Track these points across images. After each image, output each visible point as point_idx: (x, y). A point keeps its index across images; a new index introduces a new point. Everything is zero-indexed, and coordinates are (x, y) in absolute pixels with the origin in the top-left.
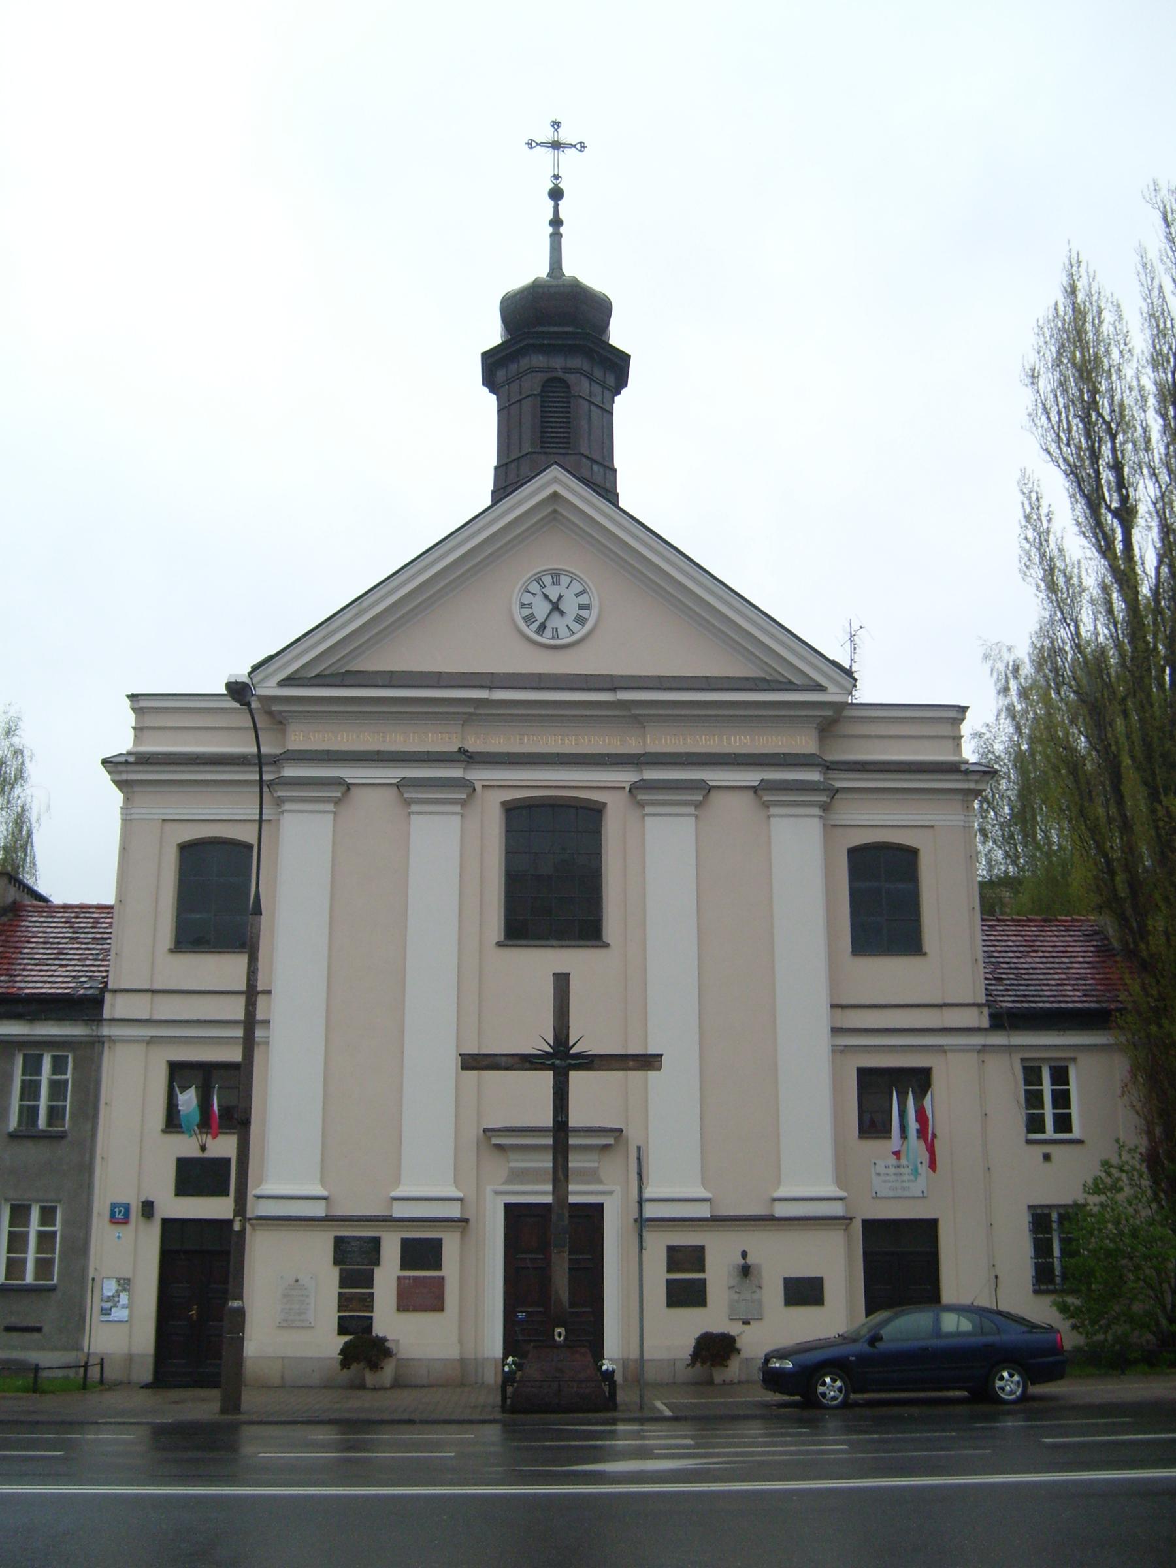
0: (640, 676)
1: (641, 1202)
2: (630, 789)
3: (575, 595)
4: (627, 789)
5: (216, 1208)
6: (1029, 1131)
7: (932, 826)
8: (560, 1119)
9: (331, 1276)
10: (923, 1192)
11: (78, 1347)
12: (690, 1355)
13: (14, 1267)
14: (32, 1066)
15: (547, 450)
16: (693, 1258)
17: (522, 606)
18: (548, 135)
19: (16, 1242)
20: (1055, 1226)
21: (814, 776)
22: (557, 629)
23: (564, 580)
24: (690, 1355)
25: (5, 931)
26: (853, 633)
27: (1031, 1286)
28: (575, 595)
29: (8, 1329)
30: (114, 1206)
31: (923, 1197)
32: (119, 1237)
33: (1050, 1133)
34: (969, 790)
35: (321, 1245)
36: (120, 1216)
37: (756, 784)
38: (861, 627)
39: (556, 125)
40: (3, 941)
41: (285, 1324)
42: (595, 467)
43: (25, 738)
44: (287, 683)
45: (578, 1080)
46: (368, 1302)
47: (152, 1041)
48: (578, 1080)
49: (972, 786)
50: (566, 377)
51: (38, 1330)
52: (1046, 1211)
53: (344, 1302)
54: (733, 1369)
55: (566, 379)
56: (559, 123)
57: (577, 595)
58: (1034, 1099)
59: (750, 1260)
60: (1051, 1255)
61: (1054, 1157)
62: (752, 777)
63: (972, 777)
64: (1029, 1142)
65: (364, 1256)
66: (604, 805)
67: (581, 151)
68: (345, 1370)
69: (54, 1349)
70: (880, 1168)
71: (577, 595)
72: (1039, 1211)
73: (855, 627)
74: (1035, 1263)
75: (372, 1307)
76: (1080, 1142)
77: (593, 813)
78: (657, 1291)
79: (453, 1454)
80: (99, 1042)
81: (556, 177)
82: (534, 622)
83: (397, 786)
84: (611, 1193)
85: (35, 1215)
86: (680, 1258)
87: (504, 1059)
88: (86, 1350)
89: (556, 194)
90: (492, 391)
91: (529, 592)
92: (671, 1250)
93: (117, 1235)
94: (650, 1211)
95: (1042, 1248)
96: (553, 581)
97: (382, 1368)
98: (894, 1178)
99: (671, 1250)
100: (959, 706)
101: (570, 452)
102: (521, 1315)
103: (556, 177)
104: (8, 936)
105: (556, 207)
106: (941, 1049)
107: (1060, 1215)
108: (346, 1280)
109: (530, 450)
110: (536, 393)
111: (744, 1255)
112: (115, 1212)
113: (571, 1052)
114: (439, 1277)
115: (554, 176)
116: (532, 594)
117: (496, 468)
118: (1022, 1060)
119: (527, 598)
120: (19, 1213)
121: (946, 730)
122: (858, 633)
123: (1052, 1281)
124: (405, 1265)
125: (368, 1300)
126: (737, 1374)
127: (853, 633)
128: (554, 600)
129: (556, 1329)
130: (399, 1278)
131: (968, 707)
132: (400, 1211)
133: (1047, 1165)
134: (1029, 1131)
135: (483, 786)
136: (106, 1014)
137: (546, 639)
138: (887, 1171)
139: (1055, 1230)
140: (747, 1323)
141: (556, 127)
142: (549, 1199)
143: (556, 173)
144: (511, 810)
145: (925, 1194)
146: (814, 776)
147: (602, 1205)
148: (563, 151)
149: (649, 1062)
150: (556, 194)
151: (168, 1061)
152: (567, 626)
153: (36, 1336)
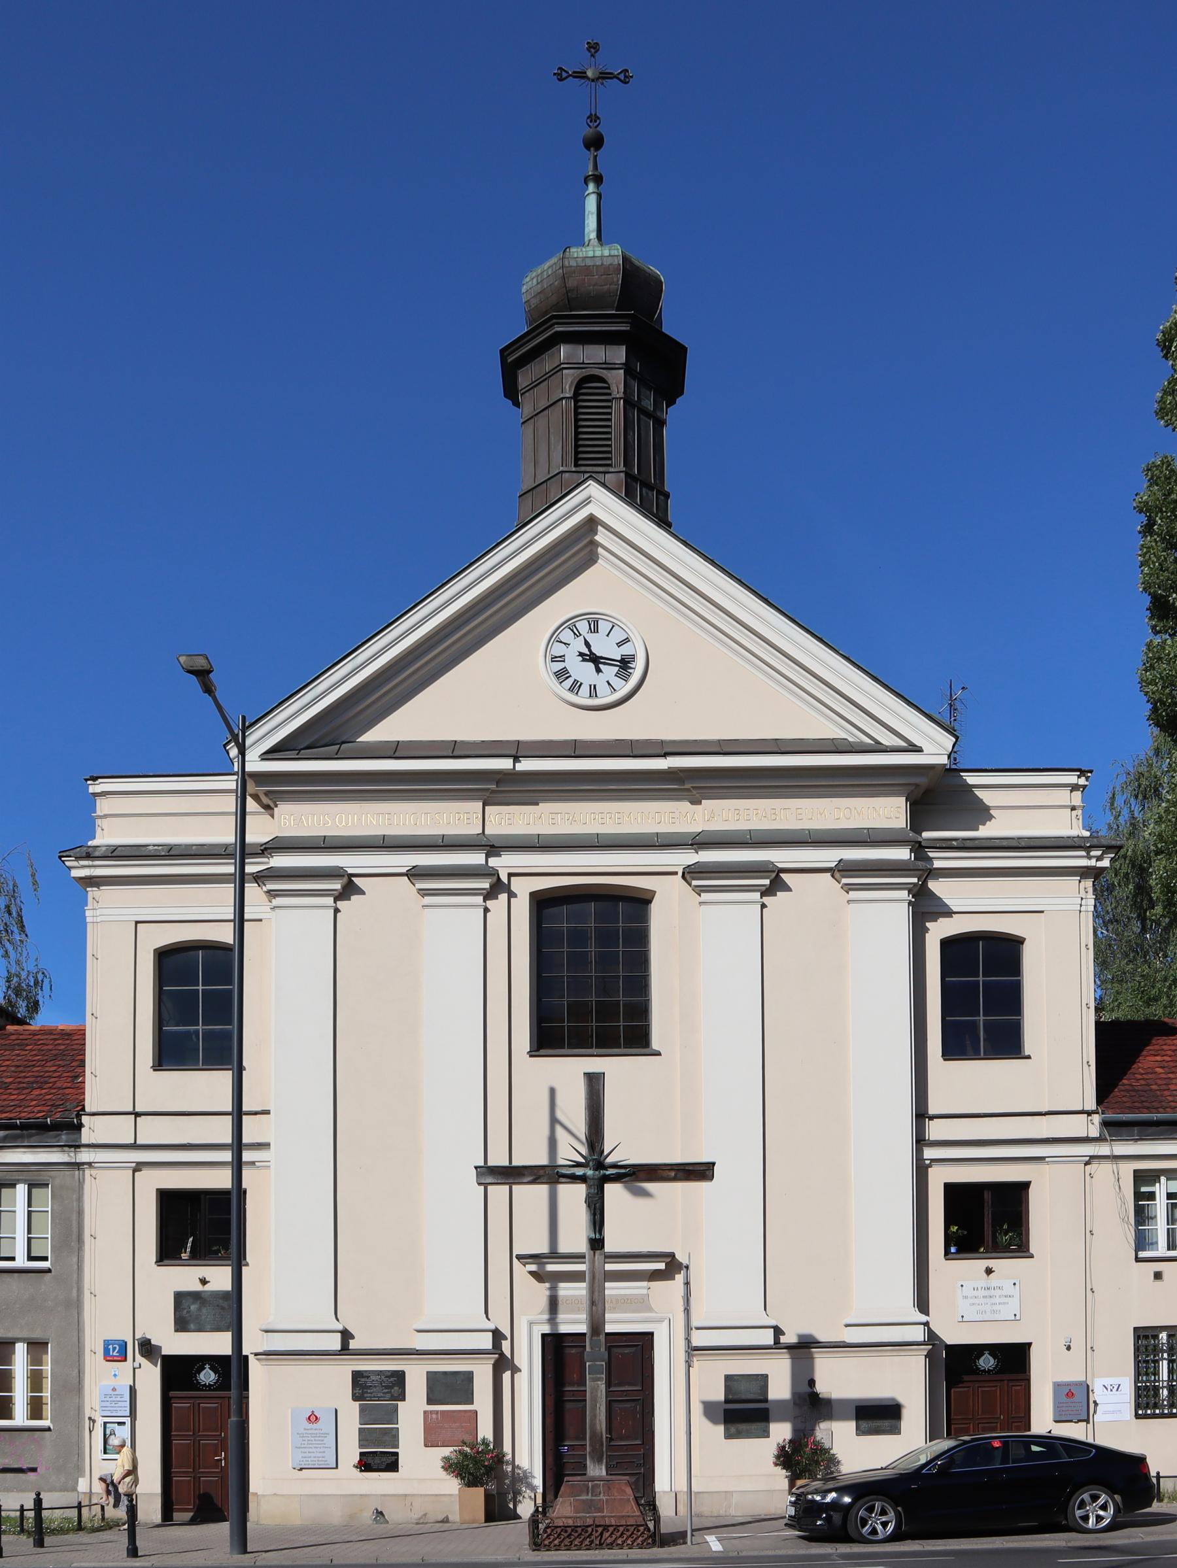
2: (683, 873)
3: (617, 644)
4: (680, 874)
5: (218, 1344)
9: (351, 1413)
10: (1015, 1315)
21: (476, 858)
22: (581, 684)
28: (617, 644)
32: (115, 1375)
35: (341, 1374)
36: (116, 1352)
44: (270, 756)
57: (619, 644)
62: (830, 856)
66: (653, 893)
71: (619, 644)
77: (640, 902)
81: (594, 118)
82: (567, 678)
91: (561, 642)
93: (113, 1373)
94: (699, 1339)
96: (590, 628)
98: (982, 1301)
109: (561, 469)
110: (568, 395)
114: (470, 1411)
115: (590, 117)
116: (565, 644)
119: (558, 650)
130: (425, 1412)
133: (1158, 1283)
137: (583, 699)
138: (975, 1293)
144: (542, 903)
145: (1018, 1318)
146: (476, 858)
147: (652, 1334)
148: (602, 84)
151: (157, 1189)
152: (608, 682)
153: (31, 1475)
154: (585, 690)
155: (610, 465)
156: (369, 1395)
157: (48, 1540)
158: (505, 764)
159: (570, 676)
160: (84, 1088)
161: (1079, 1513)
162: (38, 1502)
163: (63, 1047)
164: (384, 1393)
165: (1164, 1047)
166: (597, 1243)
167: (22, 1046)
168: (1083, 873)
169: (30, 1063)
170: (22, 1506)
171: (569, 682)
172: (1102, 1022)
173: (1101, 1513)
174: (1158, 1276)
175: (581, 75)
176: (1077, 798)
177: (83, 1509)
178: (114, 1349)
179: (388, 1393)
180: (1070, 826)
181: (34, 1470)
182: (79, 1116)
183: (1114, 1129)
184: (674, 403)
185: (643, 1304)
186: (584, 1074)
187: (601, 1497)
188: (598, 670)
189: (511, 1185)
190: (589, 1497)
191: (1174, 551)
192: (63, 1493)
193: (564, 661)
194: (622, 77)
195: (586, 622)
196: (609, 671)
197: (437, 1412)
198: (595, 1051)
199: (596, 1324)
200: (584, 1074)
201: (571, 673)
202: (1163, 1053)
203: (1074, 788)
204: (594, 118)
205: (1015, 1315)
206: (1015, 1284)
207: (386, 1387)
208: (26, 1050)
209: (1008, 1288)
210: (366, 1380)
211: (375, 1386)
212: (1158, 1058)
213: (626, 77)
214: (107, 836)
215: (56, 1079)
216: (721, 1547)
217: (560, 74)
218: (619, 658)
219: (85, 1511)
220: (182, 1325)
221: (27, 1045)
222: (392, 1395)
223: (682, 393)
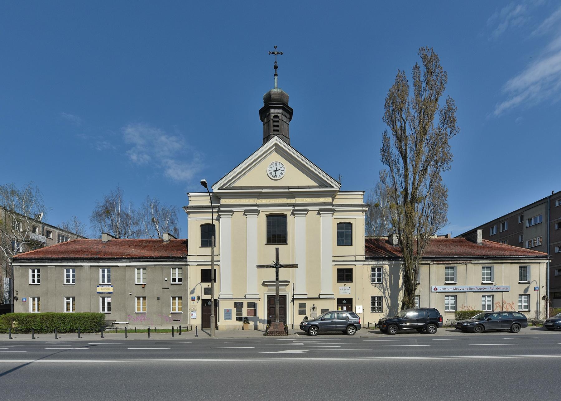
1: (293, 295)
11: (187, 324)
16: (302, 306)
17: (269, 171)
21: (331, 207)
23: (278, 164)
33: (376, 282)
35: (232, 303)
39: (275, 47)
47: (198, 265)
60: (375, 305)
67: (281, 55)
70: (341, 288)
77: (285, 216)
78: (296, 312)
81: (276, 62)
84: (288, 293)
86: (302, 306)
89: (276, 67)
106: (355, 265)
111: (314, 305)
126: (49, 272)
128: (275, 172)
132: (247, 297)
135: (262, 211)
142: (275, 295)
146: (331, 207)
149: (295, 266)
150: (276, 67)
155: (279, 133)
157: (182, 333)
158: (287, 190)
161: (349, 329)
162: (180, 327)
166: (277, 279)
167: (177, 243)
168: (363, 211)
173: (314, 333)
175: (273, 53)
176: (362, 197)
180: (361, 202)
181: (179, 320)
183: (367, 259)
185: (284, 290)
188: (274, 171)
189: (295, 268)
194: (281, 53)
196: (274, 173)
198: (277, 244)
199: (277, 293)
203: (362, 195)
204: (276, 62)
209: (348, 287)
214: (191, 204)
219: (188, 328)
220: (205, 294)
223: (292, 119)
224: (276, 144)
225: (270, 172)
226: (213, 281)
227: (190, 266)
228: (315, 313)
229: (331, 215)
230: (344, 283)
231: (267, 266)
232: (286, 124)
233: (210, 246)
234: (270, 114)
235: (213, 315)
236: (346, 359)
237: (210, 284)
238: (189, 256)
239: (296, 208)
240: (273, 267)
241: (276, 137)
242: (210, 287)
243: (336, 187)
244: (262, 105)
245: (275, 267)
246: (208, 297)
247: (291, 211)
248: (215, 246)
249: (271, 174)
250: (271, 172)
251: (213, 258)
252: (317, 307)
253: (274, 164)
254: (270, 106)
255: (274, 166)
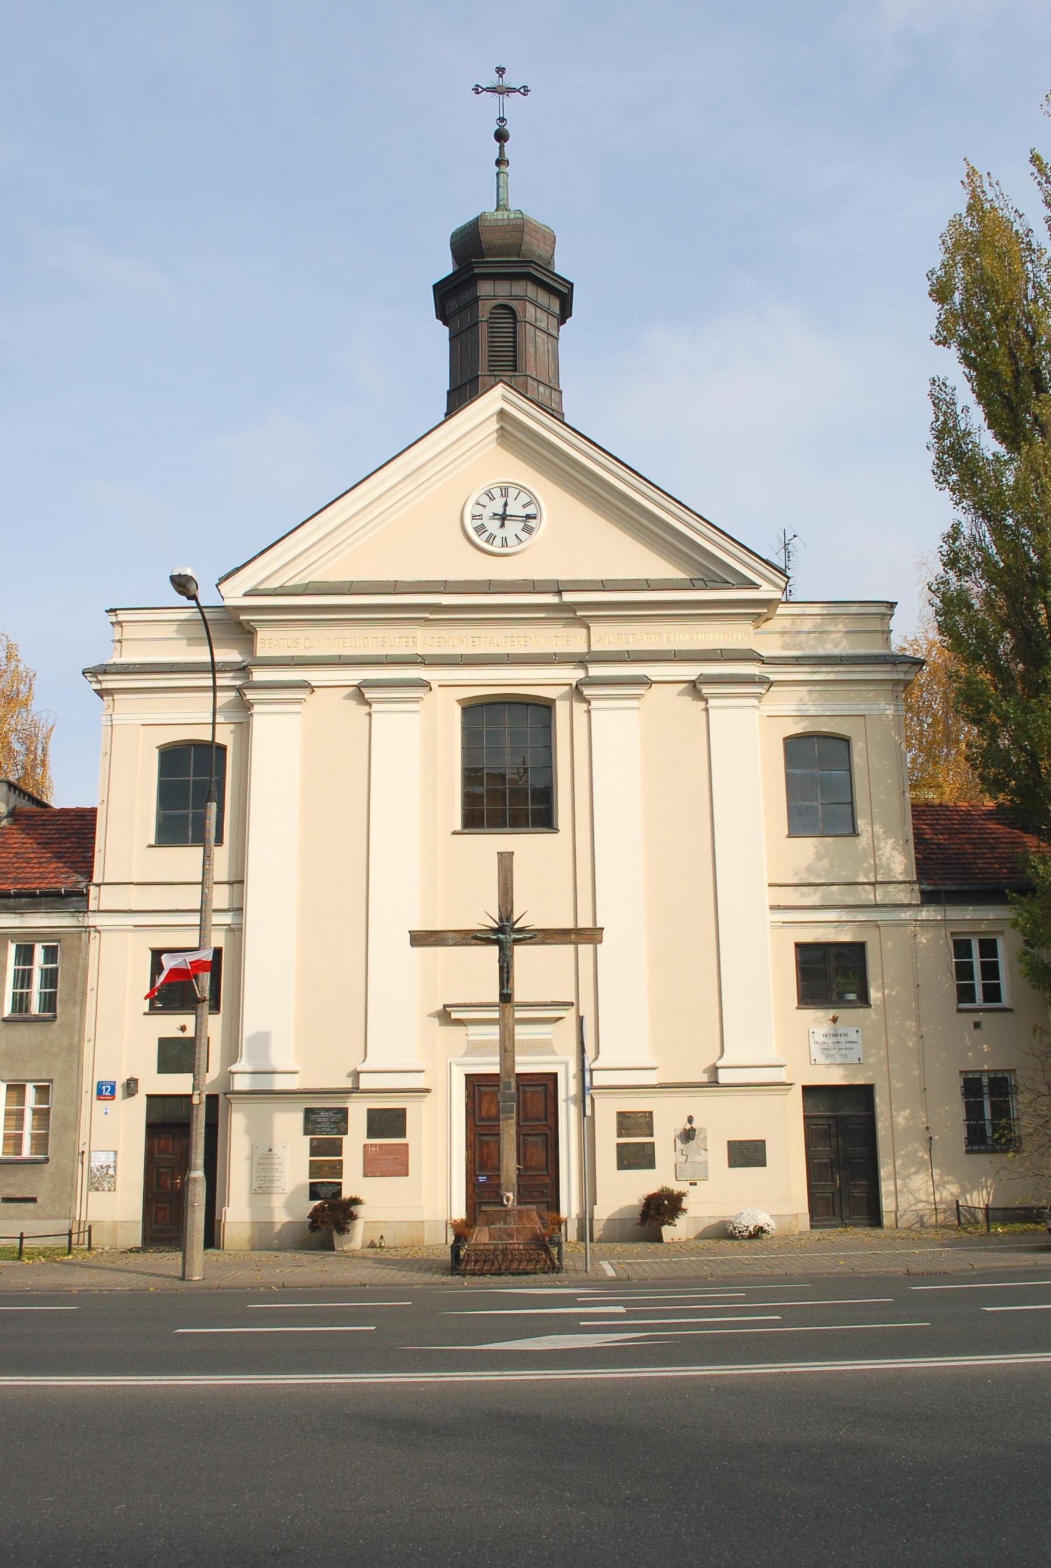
0: (584, 581)
6: (960, 1001)
7: (864, 715)
8: (503, 992)
10: (859, 1059)
11: (70, 1216)
12: (640, 1215)
13: (14, 1141)
14: (25, 954)
15: (496, 373)
16: (642, 1123)
17: (474, 517)
18: (491, 79)
19: (15, 1117)
20: (986, 1090)
22: (495, 536)
24: (640, 1215)
25: (4, 833)
26: (787, 542)
27: (964, 1147)
29: (6, 1200)
30: (100, 1085)
31: (859, 1063)
32: (106, 1113)
34: (898, 680)
36: (105, 1092)
37: (693, 678)
38: (795, 536)
39: (501, 71)
40: (2, 843)
41: (260, 1191)
42: (541, 389)
43: (27, 660)
45: (521, 954)
46: (337, 1169)
48: (521, 954)
49: (901, 676)
50: (514, 304)
51: (34, 1200)
52: (977, 1076)
53: (315, 1169)
54: (676, 1232)
55: (513, 306)
56: (504, 69)
57: (524, 506)
58: (964, 971)
59: (694, 1125)
61: (983, 1025)
62: (691, 671)
63: (900, 668)
64: (959, 1011)
65: (333, 1126)
68: (314, 1233)
69: (50, 1217)
71: (524, 506)
72: (971, 1076)
73: (789, 536)
74: (968, 1125)
75: (341, 1173)
76: (1009, 1010)
77: (546, 707)
79: (373, 1328)
80: (86, 931)
81: (502, 119)
82: (485, 532)
83: (358, 687)
85: (30, 1091)
86: (627, 1122)
87: (450, 934)
88: (77, 1218)
89: (501, 136)
90: (445, 323)
92: (622, 1116)
95: (973, 1111)
96: (502, 494)
97: (349, 1231)
99: (622, 1116)
100: (888, 602)
101: (517, 374)
102: (482, 1179)
103: (502, 119)
104: (6, 838)
105: (501, 148)
107: (990, 1079)
108: (315, 1149)
111: (690, 1120)
112: (102, 1090)
113: (516, 926)
115: (499, 119)
116: (483, 506)
117: (449, 393)
118: (952, 934)
120: (16, 1089)
121: (876, 625)
122: (792, 542)
123: (983, 1142)
124: (371, 1134)
125: (338, 1167)
127: (787, 542)
129: (511, 1193)
130: (365, 1146)
131: (896, 603)
132: (365, 1082)
134: (960, 1001)
136: (92, 906)
139: (986, 1094)
140: (693, 1184)
141: (500, 73)
142: (496, 1070)
143: (501, 116)
145: (861, 1062)
148: (508, 95)
150: (501, 136)
152: (516, 535)
153: (31, 1205)
154: (498, 541)
155: (515, 370)
156: (319, 1130)
159: (486, 531)
160: (93, 862)
163: (77, 827)
164: (331, 1128)
165: (972, 827)
166: (506, 997)
169: (51, 841)
170: (22, 1234)
171: (486, 535)
172: (1038, 764)
174: (977, 1025)
177: (73, 1236)
178: (107, 1089)
179: (335, 1128)
182: (87, 886)
183: (929, 898)
184: (565, 322)
185: (544, 1047)
186: (498, 853)
187: (512, 1226)
190: (502, 1226)
191: (1004, 378)
192: (57, 1221)
193: (482, 519)
195: (499, 489)
197: (376, 1145)
200: (498, 853)
201: (487, 528)
202: (970, 831)
205: (859, 1059)
206: (857, 1031)
207: (334, 1123)
208: (47, 829)
210: (317, 1116)
211: (324, 1122)
212: (967, 836)
213: (525, 91)
215: (71, 854)
216: (613, 1272)
217: (477, 89)
218: (524, 515)
219: (74, 1237)
221: (49, 825)
222: (339, 1130)
224: (502, 414)
225: (478, 523)
226: (206, 1006)
227: (99, 932)
228: (699, 1158)
229: (754, 702)
230: (831, 1013)
231: (458, 936)
232: (545, 336)
233: (199, 838)
234: (477, 299)
235: (198, 1173)
236: (778, 1370)
237: (189, 1020)
238: (98, 885)
239: (596, 671)
240: (488, 942)
241: (500, 390)
242: (190, 1033)
243: (765, 586)
244: (446, 267)
245: (497, 942)
246: (179, 1084)
247: (571, 685)
248: (219, 841)
249: (480, 529)
250: (479, 522)
251: (205, 898)
252: (704, 1130)
253: (496, 493)
254: (476, 271)
255: (492, 499)
